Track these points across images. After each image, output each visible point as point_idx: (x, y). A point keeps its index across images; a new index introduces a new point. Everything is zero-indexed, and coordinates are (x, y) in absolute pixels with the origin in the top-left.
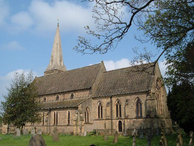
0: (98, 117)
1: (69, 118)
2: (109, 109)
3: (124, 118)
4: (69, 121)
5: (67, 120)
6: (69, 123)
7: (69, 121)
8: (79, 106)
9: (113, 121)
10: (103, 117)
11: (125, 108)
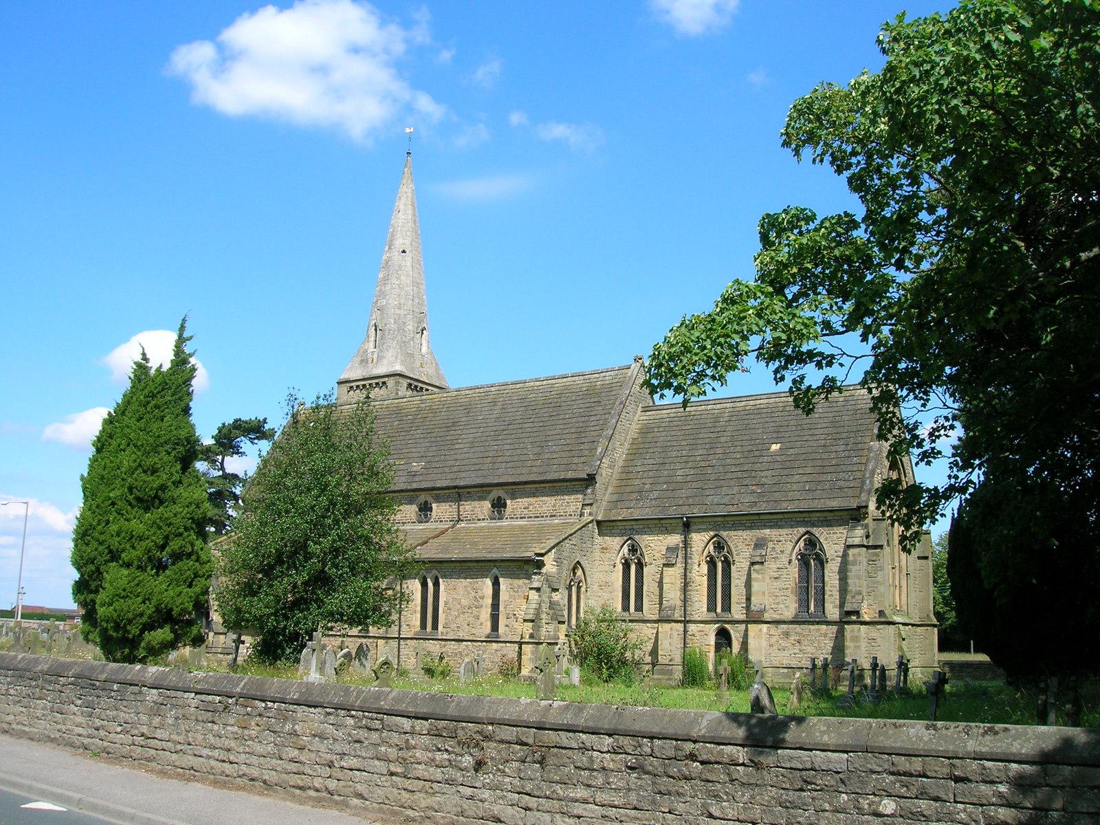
1: (495, 606)
2: (673, 576)
3: (743, 617)
5: (486, 613)
6: (495, 627)
11: (749, 575)
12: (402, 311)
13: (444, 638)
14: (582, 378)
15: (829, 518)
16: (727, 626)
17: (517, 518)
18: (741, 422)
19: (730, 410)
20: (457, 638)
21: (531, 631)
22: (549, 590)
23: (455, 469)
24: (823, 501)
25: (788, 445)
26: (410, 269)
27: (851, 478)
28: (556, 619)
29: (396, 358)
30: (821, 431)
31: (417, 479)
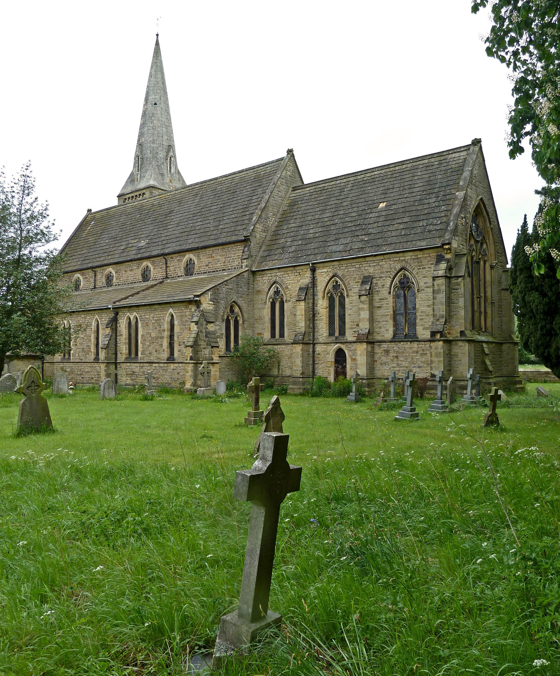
0: (270, 334)
1: (171, 337)
4: (171, 346)
5: (165, 343)
7: (171, 346)
8: (202, 299)
9: (318, 348)
10: (286, 334)
12: (155, 145)
13: (142, 361)
14: (252, 171)
15: (419, 256)
16: (343, 347)
17: (201, 273)
18: (359, 190)
19: (353, 182)
20: (149, 361)
21: (191, 355)
22: (204, 323)
23: (165, 242)
24: (414, 242)
25: (392, 202)
26: (160, 115)
27: (439, 222)
28: (210, 345)
29: (151, 176)
30: (418, 189)
31: (141, 251)
